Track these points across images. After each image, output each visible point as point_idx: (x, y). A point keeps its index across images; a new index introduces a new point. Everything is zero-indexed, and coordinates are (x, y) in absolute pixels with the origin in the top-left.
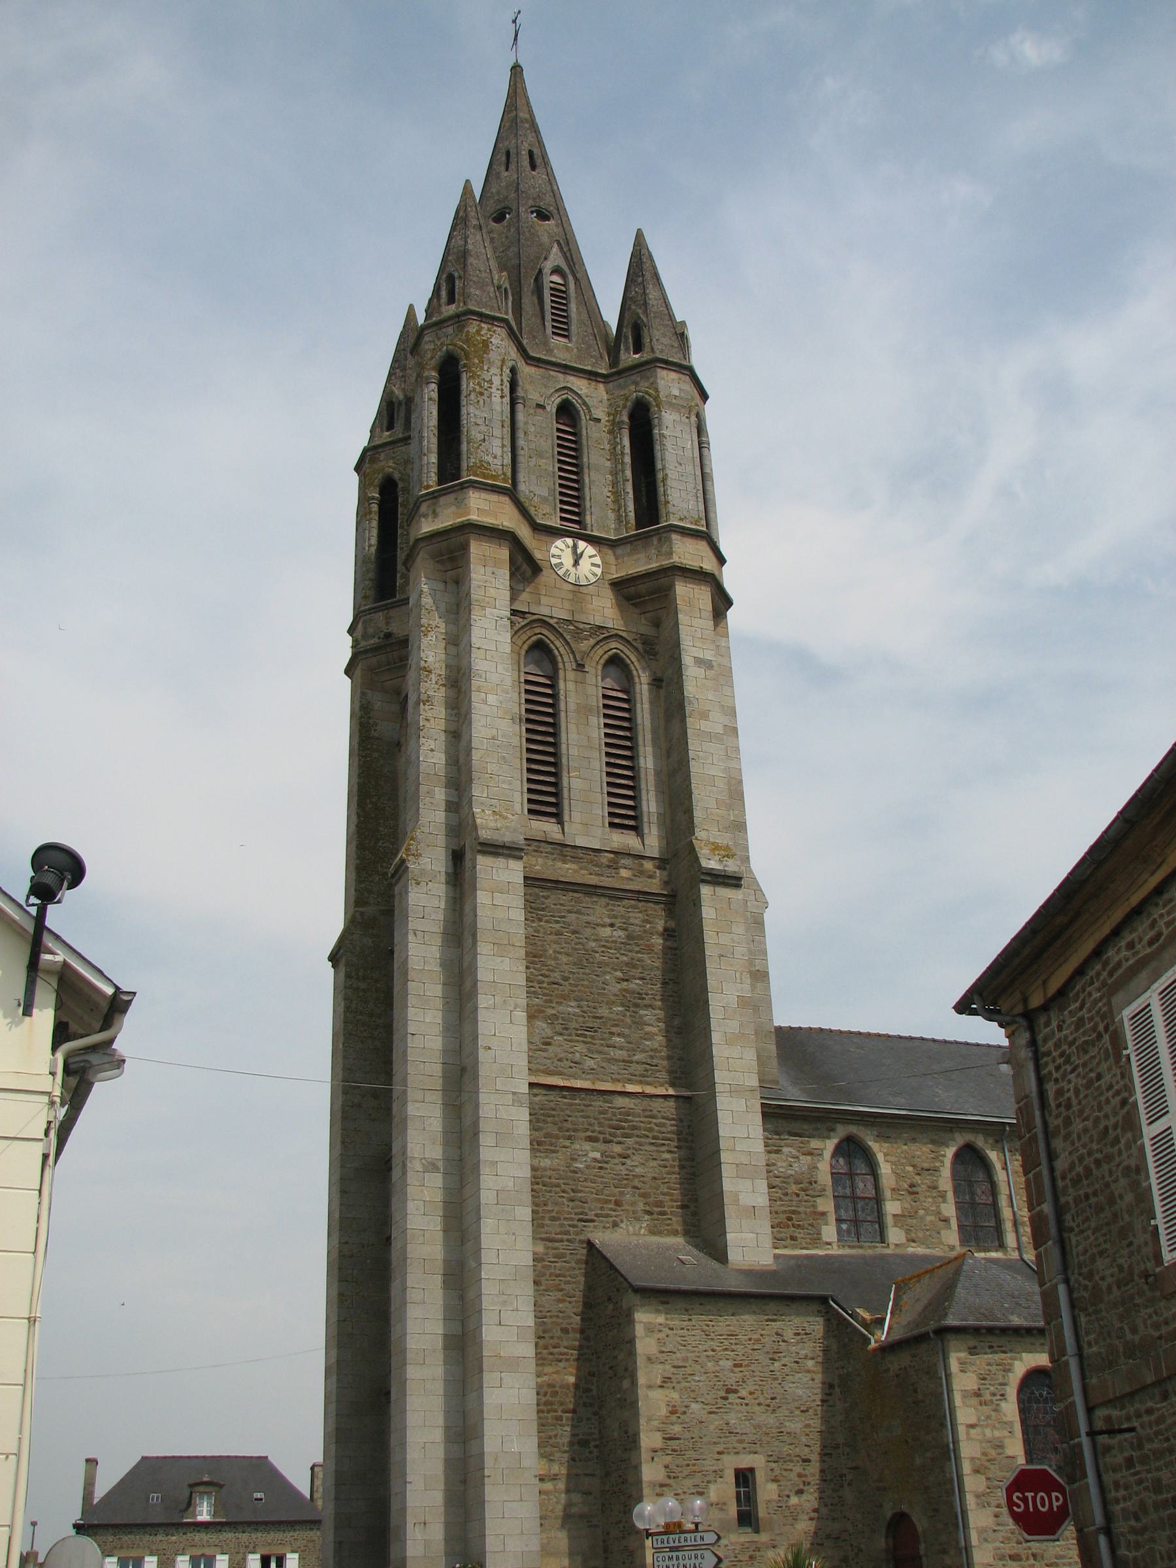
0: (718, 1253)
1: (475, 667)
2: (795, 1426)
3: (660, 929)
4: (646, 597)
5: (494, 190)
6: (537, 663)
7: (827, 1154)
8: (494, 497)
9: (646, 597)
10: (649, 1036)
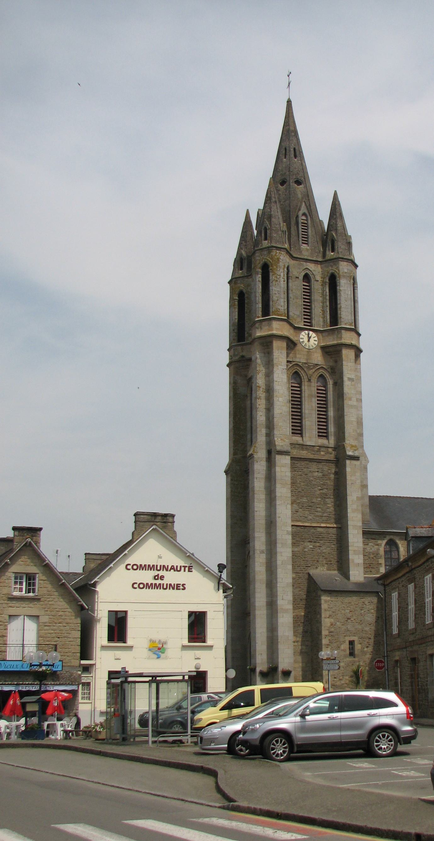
0: (347, 577)
1: (275, 388)
2: (367, 629)
3: (333, 472)
4: (332, 353)
5: (280, 168)
6: (295, 379)
7: (383, 545)
8: (281, 323)
9: (332, 353)
10: (328, 508)
